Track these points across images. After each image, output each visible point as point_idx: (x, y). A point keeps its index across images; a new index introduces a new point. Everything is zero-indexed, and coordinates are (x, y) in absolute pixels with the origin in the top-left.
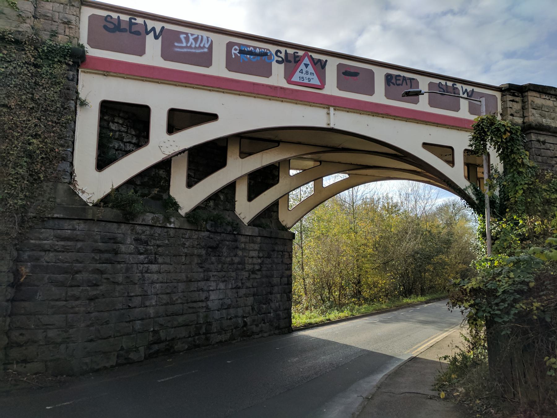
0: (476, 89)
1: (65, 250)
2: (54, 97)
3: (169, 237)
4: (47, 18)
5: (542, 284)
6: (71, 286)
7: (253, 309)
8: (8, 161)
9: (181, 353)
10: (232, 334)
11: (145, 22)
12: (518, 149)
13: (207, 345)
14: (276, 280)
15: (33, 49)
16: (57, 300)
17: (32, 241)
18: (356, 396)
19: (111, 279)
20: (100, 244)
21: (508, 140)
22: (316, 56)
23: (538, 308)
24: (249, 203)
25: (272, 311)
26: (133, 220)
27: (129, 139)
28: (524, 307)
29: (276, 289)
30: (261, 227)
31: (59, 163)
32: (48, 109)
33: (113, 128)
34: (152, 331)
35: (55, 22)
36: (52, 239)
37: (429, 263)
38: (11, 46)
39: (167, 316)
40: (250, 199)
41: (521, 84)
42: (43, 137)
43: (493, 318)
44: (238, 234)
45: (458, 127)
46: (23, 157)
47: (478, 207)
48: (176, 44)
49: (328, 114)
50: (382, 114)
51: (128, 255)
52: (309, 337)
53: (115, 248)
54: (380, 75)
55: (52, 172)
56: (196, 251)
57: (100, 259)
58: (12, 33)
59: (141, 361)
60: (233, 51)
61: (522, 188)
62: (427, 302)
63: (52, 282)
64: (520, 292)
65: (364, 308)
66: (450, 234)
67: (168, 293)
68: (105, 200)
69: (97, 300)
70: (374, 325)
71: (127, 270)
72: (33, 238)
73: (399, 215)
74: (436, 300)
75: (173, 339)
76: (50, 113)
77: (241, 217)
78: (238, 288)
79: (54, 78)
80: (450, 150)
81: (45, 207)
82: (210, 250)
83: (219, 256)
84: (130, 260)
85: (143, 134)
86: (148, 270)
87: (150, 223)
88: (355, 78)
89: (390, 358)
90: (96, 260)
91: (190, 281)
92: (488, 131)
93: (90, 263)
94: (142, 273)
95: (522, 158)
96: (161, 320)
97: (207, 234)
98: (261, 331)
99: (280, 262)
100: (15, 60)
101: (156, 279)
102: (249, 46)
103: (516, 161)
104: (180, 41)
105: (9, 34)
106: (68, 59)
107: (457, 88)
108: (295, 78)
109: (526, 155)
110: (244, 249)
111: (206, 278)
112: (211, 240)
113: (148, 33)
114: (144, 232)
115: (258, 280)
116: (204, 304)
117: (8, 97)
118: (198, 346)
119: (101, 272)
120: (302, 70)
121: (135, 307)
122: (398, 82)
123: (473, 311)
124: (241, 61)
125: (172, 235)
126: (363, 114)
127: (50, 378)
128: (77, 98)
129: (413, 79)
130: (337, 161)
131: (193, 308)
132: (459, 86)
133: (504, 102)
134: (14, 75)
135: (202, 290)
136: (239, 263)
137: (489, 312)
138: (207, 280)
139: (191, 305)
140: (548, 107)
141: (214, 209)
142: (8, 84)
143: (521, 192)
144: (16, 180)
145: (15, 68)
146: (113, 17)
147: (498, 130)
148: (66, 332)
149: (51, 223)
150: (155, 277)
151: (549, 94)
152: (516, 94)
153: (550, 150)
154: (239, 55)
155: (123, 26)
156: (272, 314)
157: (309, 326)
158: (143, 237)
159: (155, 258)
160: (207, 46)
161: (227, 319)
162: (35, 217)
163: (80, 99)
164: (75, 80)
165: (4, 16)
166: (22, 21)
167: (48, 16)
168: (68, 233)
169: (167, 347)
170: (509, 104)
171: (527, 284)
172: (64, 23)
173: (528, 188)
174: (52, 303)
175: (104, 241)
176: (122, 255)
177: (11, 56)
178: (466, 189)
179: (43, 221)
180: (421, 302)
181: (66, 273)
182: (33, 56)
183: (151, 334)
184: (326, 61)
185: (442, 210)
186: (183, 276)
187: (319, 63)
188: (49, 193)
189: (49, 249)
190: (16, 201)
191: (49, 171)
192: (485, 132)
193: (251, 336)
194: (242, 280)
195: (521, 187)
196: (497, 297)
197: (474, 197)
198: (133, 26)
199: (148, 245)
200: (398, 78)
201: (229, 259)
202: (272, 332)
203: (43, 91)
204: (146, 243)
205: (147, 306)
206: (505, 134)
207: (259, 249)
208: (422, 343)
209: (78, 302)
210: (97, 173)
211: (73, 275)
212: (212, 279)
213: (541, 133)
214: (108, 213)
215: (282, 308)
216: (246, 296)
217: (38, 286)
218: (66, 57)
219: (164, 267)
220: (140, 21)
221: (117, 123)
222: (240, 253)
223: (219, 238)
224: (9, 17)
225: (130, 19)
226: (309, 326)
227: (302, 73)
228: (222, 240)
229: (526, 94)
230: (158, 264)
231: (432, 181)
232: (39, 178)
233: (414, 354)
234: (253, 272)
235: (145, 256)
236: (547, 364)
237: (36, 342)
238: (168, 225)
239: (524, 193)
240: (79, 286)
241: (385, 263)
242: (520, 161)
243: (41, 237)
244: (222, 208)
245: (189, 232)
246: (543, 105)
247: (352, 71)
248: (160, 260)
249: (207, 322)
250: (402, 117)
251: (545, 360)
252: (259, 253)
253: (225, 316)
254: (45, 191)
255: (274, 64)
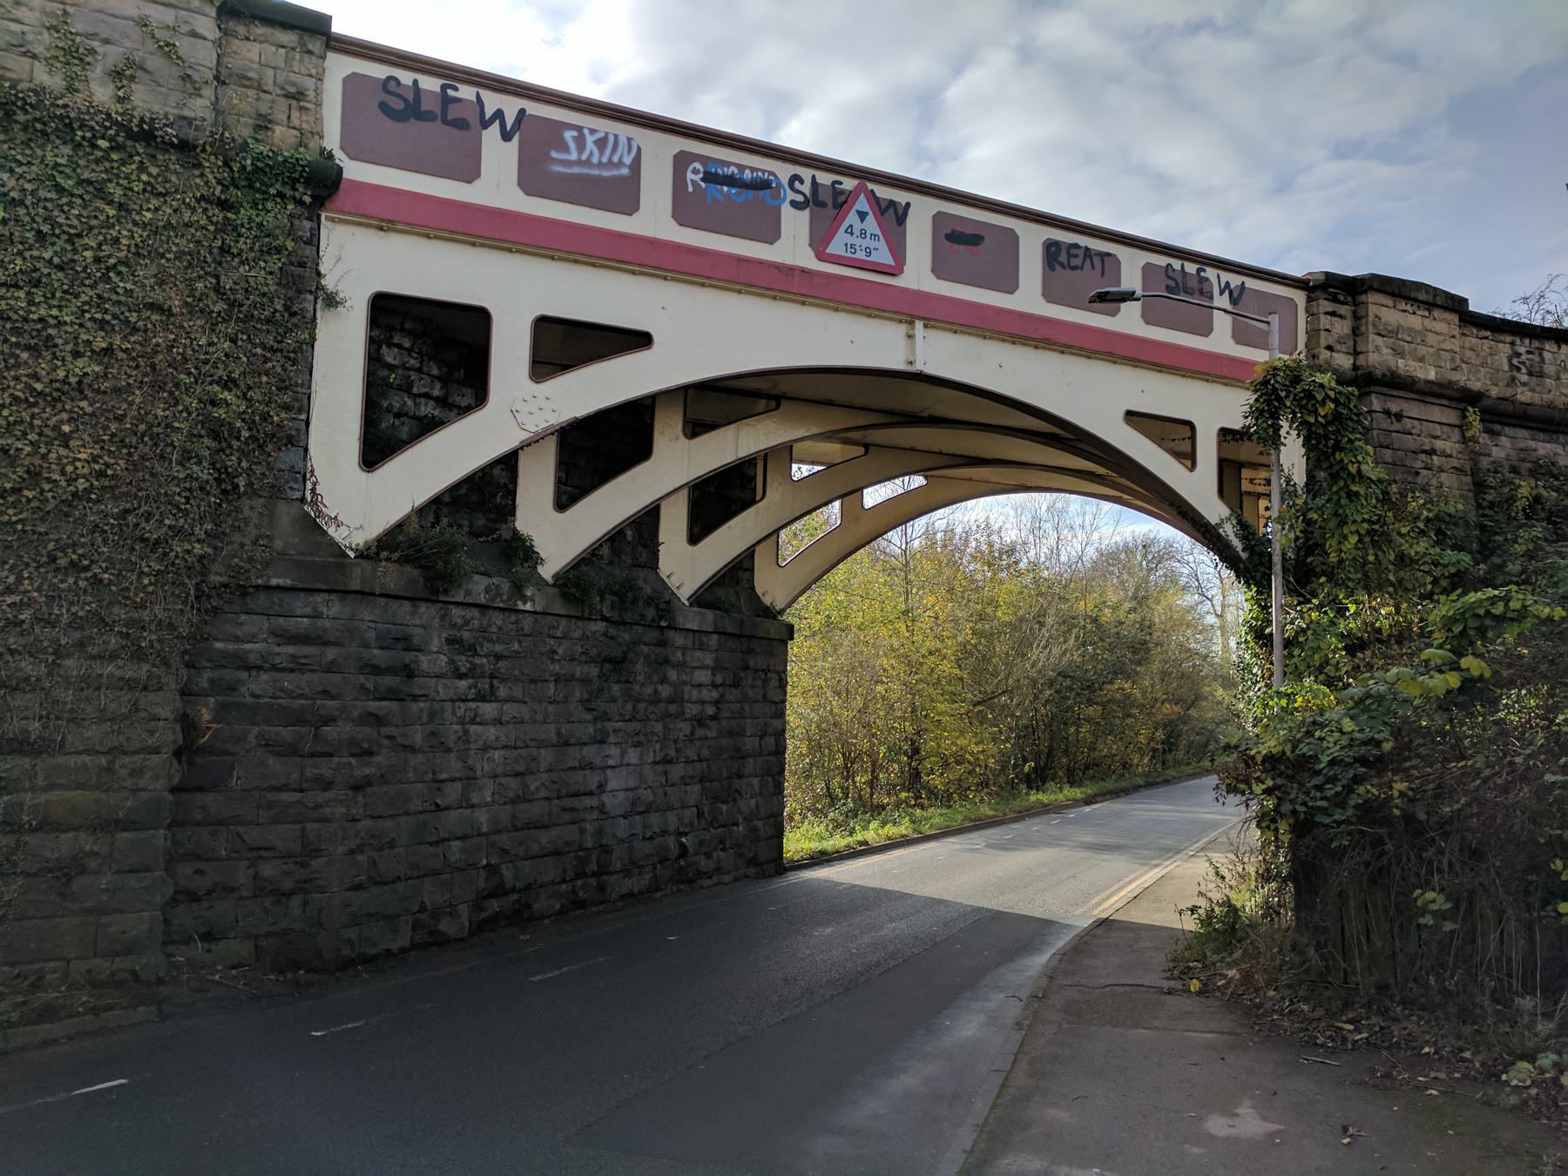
0: (1251, 283)
1: (297, 666)
2: (267, 285)
3: (521, 634)
4: (248, 83)
5: (1408, 747)
6: (313, 755)
7: (700, 814)
8: (167, 445)
9: (546, 921)
10: (655, 875)
11: (478, 95)
12: (1351, 441)
13: (602, 903)
14: (750, 743)
15: (220, 163)
16: (278, 789)
17: (218, 645)
18: (1002, 996)
19: (399, 739)
20: (376, 652)
21: (1330, 418)
22: (883, 192)
23: (1402, 794)
24: (690, 548)
25: (741, 821)
26: (446, 592)
27: (424, 386)
28: (1374, 790)
29: (751, 765)
30: (719, 609)
31: (280, 449)
32: (252, 316)
33: (390, 360)
34: (484, 867)
35: (264, 92)
36: (265, 640)
37: (1090, 702)
38: (167, 157)
39: (516, 830)
40: (694, 539)
41: (1351, 273)
42: (242, 385)
43: (1313, 816)
44: (669, 627)
45: (1209, 374)
46: (201, 436)
47: (1246, 568)
48: (554, 155)
49: (910, 337)
50: (1033, 339)
51: (434, 680)
52: (831, 885)
53: (407, 661)
54: (1032, 240)
55: (264, 474)
56: (578, 669)
57: (376, 689)
58: (172, 124)
59: (462, 940)
60: (690, 176)
61: (1357, 531)
62: (1088, 801)
63: (266, 744)
64: (1363, 761)
65: (936, 816)
66: (1147, 627)
67: (518, 774)
68: (391, 542)
69: (369, 790)
70: (978, 855)
71: (433, 715)
72: (220, 636)
73: (1020, 574)
74: (1108, 796)
75: (527, 888)
76: (259, 326)
77: (673, 583)
78: (667, 761)
79: (268, 236)
80: (1187, 432)
81: (250, 560)
82: (608, 666)
83: (627, 681)
84: (438, 692)
85: (457, 375)
86: (475, 716)
87: (482, 599)
88: (974, 249)
89: (1041, 928)
90: (367, 690)
91: (567, 744)
92: (1287, 397)
93: (356, 699)
94: (463, 724)
95: (1358, 462)
96: (504, 840)
97: (600, 626)
98: (718, 870)
99: (760, 698)
100: (176, 191)
101: (493, 737)
102: (729, 164)
103: (1344, 468)
104: (564, 148)
105: (166, 125)
106: (301, 189)
107: (1207, 279)
108: (836, 247)
109: (1367, 453)
110: (681, 665)
111: (599, 738)
112: (611, 642)
113: (486, 124)
114: (467, 623)
115: (712, 743)
116: (595, 803)
117: (161, 283)
118: (582, 904)
119: (377, 720)
120: (851, 226)
121: (448, 808)
122: (1076, 262)
123: (1270, 803)
124: (709, 200)
125: (527, 629)
126: (990, 338)
127: (272, 977)
128: (320, 288)
129: (1109, 255)
130: (925, 448)
131: (573, 810)
132: (1211, 273)
133: (1312, 315)
134: (173, 228)
135: (591, 766)
136: (671, 701)
137: (1304, 804)
138: (602, 742)
139: (568, 802)
140: (1411, 330)
141: (611, 562)
142: (161, 250)
143: (1354, 539)
144: (188, 494)
145: (175, 211)
146: (403, 81)
147: (1309, 395)
148: (303, 865)
149: (262, 600)
150: (491, 733)
151: (1416, 300)
152: (1341, 298)
153: (1411, 434)
154: (703, 185)
155: (426, 106)
156: (741, 828)
157: (821, 858)
158: (466, 635)
159: (492, 686)
160: (628, 160)
161: (644, 838)
162: (225, 586)
163: (323, 288)
164: (315, 242)
165: (147, 77)
166: (192, 91)
167: (250, 79)
168: (302, 623)
169: (517, 906)
170: (1325, 321)
171: (1378, 744)
172: (288, 96)
173: (1368, 532)
174: (270, 796)
175: (384, 645)
176: (421, 680)
177: (167, 181)
178: (1219, 525)
179: (245, 594)
180: (1074, 800)
181: (301, 722)
182: (219, 182)
183: (482, 873)
184: (908, 205)
185: (1113, 559)
186: (550, 732)
187: (891, 210)
188: (255, 525)
189: (258, 662)
190: (187, 546)
191: (258, 470)
192: (1279, 399)
193: (695, 881)
194: (676, 741)
195: (1353, 528)
196: (1318, 773)
197: (1237, 544)
198: (450, 106)
199: (476, 654)
200: (1074, 251)
201: (649, 690)
202: (741, 872)
203: (241, 270)
204: (472, 649)
205: (473, 806)
206: (1323, 403)
207: (712, 664)
208: (1109, 892)
209: (329, 795)
210: (363, 476)
211: (317, 729)
212: (612, 739)
213: (1395, 393)
214: (391, 575)
215: (762, 812)
216: (686, 781)
217: (232, 754)
218: (298, 185)
219: (511, 710)
220: (466, 92)
221: (399, 346)
222: (673, 675)
223: (627, 637)
224: (161, 81)
225: (444, 87)
226: (821, 858)
227: (852, 234)
228: (634, 643)
229: (1363, 298)
230: (497, 701)
231: (1125, 497)
232: (236, 487)
233: (1103, 911)
234: (700, 721)
235: (471, 681)
236: (1419, 903)
237: (233, 890)
238: (520, 606)
239: (1360, 541)
240: (332, 755)
241: (986, 701)
242: (1353, 469)
243: (239, 633)
244: (629, 561)
245: (563, 621)
246: (1399, 327)
247: (969, 231)
248: (502, 692)
249: (601, 846)
250: (1081, 349)
251: (1415, 895)
252: (713, 675)
253: (639, 830)
254: (246, 521)
255: (786, 210)
